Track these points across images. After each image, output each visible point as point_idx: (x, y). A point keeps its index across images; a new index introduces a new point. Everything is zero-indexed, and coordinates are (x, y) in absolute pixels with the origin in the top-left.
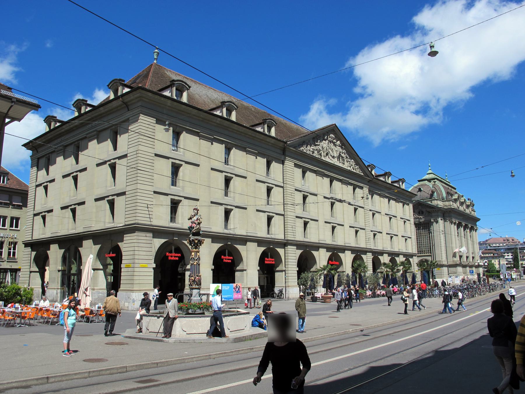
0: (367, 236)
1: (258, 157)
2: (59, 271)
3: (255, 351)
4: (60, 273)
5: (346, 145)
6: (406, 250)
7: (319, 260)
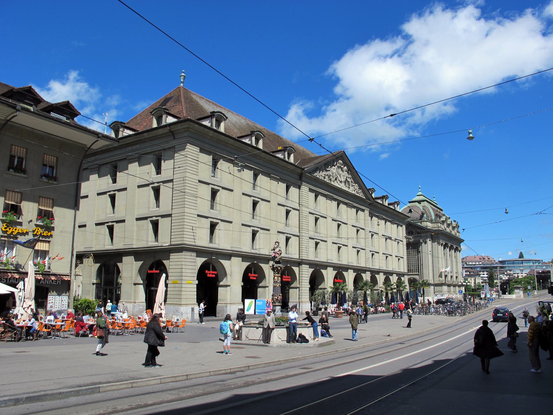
0: (367, 256)
1: (279, 182)
2: (93, 284)
3: (339, 353)
4: (95, 286)
5: (351, 170)
6: (387, 267)
7: (327, 279)
